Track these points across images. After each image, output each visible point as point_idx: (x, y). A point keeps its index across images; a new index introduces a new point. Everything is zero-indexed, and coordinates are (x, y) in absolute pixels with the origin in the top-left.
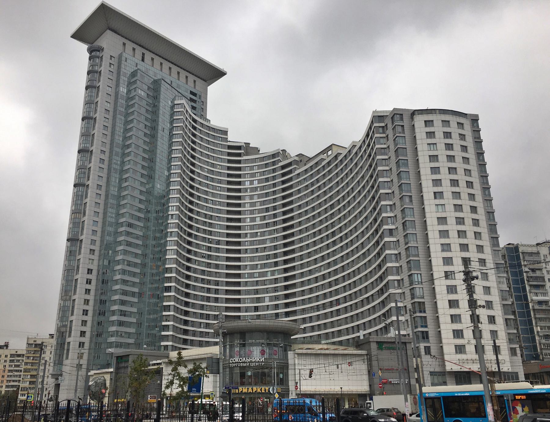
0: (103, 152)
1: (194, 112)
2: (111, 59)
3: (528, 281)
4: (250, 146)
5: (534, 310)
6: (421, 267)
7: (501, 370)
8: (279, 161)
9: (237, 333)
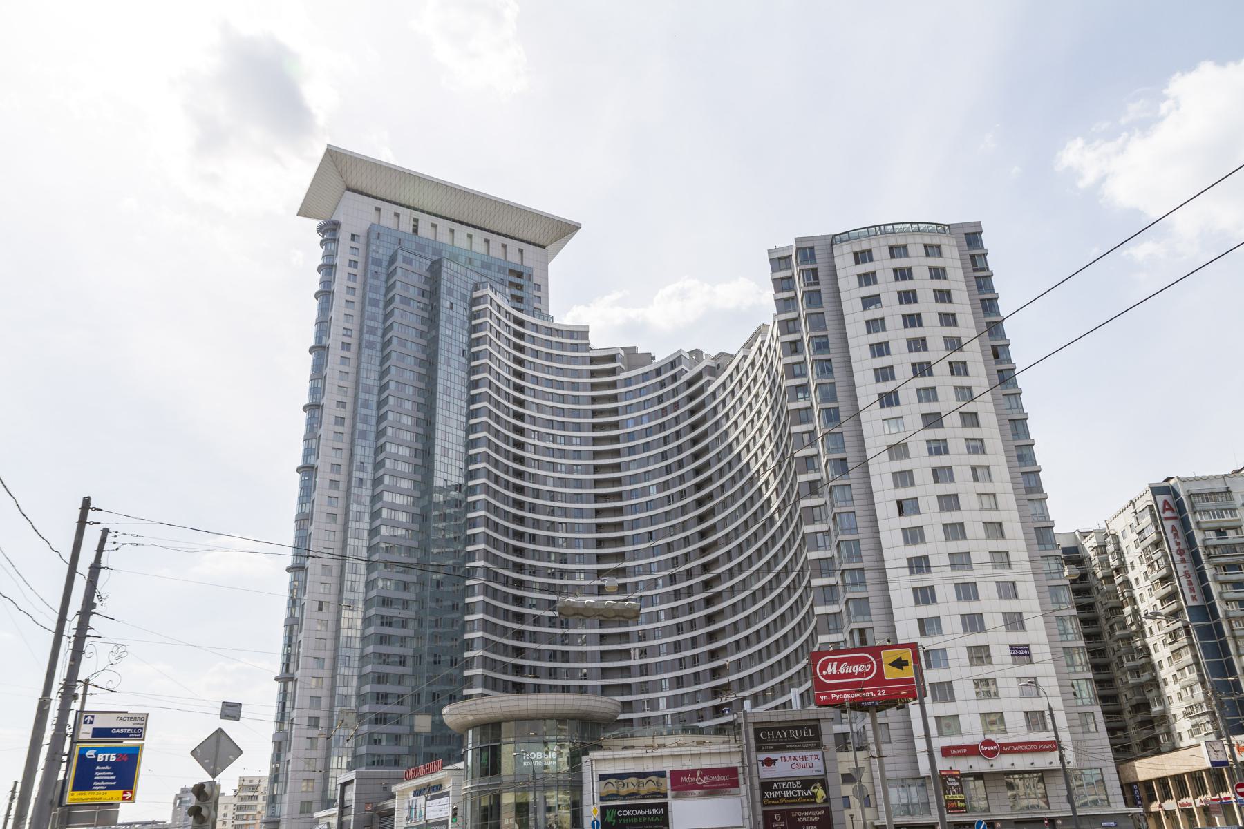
0: (341, 404)
1: (519, 306)
2: (353, 240)
3: (1209, 556)
4: (640, 351)
5: (1229, 619)
6: (863, 553)
7: (1068, 766)
8: (683, 372)
9: (551, 718)
